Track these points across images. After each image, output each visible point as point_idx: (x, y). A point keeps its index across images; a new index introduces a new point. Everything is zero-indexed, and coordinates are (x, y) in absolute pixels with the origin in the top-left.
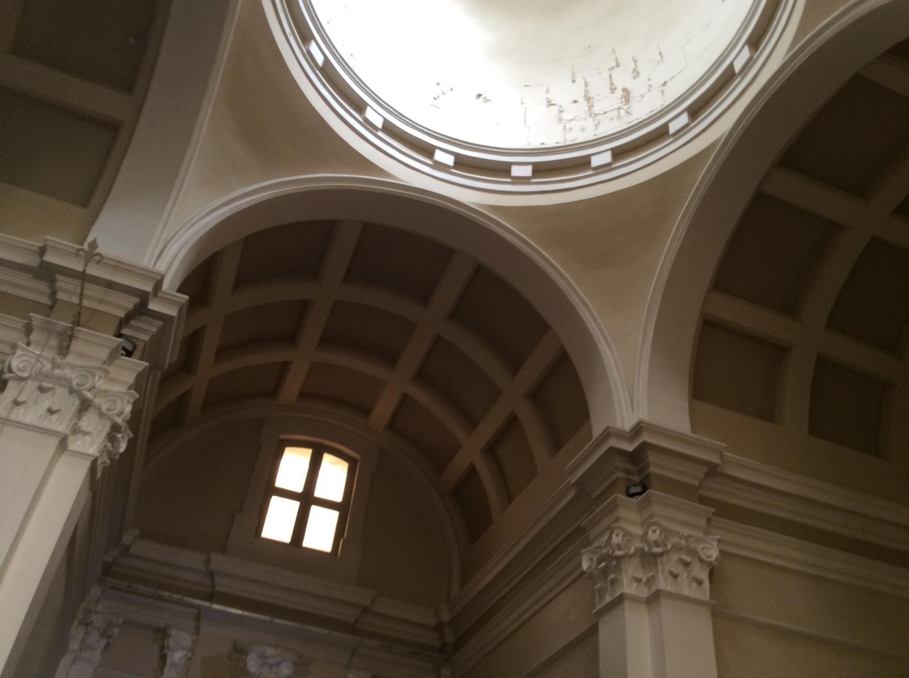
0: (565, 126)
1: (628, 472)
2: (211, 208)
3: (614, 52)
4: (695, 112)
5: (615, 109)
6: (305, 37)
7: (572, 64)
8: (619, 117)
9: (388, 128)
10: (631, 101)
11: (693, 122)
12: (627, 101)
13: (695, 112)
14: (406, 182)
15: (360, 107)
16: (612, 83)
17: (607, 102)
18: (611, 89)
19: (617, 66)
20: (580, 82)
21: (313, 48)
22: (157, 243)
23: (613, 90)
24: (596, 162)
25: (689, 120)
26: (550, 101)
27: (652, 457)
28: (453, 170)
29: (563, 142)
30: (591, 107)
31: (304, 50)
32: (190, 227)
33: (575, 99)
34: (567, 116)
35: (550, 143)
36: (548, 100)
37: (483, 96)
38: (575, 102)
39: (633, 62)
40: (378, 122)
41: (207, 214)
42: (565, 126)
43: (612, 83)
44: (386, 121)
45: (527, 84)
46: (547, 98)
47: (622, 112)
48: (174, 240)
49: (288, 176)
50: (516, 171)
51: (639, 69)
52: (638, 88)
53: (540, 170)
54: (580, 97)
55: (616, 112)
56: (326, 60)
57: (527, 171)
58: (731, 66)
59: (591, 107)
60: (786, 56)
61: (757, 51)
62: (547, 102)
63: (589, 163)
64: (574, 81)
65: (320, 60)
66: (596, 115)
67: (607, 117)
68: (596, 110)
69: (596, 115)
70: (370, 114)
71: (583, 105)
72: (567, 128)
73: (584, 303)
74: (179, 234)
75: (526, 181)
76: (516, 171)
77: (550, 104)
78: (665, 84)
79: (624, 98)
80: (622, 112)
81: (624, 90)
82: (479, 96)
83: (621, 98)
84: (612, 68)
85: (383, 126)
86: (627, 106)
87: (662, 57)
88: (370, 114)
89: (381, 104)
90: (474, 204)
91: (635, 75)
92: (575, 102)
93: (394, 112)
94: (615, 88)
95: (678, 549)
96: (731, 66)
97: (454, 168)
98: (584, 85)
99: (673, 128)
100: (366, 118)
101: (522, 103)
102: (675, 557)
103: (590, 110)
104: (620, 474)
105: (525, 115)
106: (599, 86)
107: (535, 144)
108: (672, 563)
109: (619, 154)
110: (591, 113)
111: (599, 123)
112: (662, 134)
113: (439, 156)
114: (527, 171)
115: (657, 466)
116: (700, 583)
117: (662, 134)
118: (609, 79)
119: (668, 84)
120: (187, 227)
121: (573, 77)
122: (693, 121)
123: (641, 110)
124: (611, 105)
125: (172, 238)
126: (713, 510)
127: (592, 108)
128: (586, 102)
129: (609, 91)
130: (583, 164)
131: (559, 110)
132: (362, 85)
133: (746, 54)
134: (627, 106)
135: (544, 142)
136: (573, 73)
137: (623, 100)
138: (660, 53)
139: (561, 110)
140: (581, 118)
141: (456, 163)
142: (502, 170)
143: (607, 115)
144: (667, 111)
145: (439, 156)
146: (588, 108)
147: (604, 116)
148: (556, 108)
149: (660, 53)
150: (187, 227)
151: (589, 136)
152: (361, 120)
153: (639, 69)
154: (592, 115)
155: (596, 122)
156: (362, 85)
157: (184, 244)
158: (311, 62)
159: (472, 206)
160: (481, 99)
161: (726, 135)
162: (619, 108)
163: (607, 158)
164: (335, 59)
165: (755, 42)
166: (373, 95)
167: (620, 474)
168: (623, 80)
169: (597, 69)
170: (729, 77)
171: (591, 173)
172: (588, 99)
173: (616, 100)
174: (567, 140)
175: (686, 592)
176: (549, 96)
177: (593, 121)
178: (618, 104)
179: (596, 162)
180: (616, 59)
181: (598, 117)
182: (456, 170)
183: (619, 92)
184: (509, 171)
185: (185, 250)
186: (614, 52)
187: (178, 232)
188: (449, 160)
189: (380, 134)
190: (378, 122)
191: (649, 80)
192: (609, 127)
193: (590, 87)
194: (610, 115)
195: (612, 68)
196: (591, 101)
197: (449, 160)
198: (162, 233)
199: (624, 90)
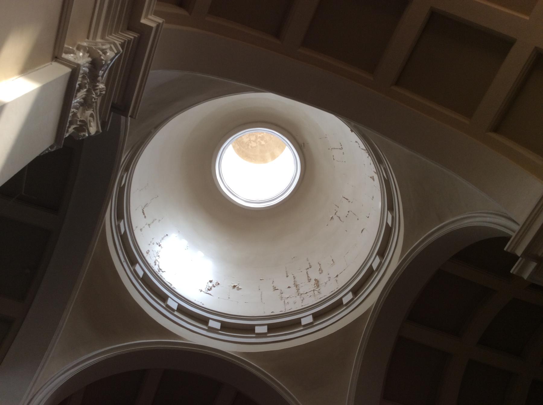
0: (284, 301)
2: (66, 369)
3: (308, 260)
4: (356, 291)
5: (312, 291)
6: (133, 262)
7: (286, 267)
8: (315, 295)
9: (180, 309)
10: (320, 286)
11: (356, 297)
12: (318, 286)
13: (356, 291)
14: (191, 341)
15: (164, 298)
16: (308, 277)
17: (307, 287)
18: (308, 280)
19: (310, 267)
20: (291, 276)
21: (137, 268)
22: (29, 394)
23: (309, 280)
24: (304, 322)
25: (353, 296)
26: (275, 288)
28: (220, 332)
29: (284, 311)
30: (298, 290)
31: (132, 270)
32: (51, 383)
33: (289, 286)
34: (285, 295)
35: (277, 312)
36: (274, 287)
37: (237, 287)
38: (289, 287)
39: (319, 265)
40: (175, 306)
41: (63, 374)
42: (284, 301)
43: (308, 277)
44: (179, 305)
45: (262, 279)
46: (273, 286)
47: (316, 292)
48: (38, 394)
49: (117, 344)
50: (258, 330)
51: (322, 269)
52: (323, 279)
53: (272, 328)
54: (292, 285)
55: (312, 292)
56: (145, 273)
57: (264, 329)
58: (371, 266)
59: (298, 290)
60: (399, 261)
61: (383, 259)
62: (274, 288)
63: (300, 323)
64: (287, 276)
65: (141, 274)
66: (301, 294)
67: (308, 295)
68: (301, 291)
69: (301, 294)
70: (170, 302)
71: (294, 289)
72: (286, 302)
74: (42, 390)
75: (265, 335)
76: (258, 330)
77: (275, 289)
78: (337, 276)
79: (316, 284)
80: (316, 292)
81: (315, 280)
82: (234, 286)
83: (315, 285)
84: (308, 269)
85: (178, 308)
86: (318, 289)
87: (334, 262)
88: (170, 302)
89: (135, 344)
90: (232, 352)
91: (321, 272)
92: (289, 287)
93: (184, 299)
94: (310, 279)
96: (371, 266)
97: (220, 330)
98: (293, 278)
99: (345, 301)
100: (168, 304)
101: (259, 289)
103: (298, 291)
105: (261, 296)
106: (302, 279)
107: (268, 314)
109: (317, 316)
110: (298, 294)
111: (304, 299)
112: (339, 305)
113: (212, 324)
114: (264, 329)
117: (339, 305)
118: (306, 274)
119: (338, 276)
120: (49, 383)
121: (287, 274)
122: (356, 296)
123: (326, 291)
124: (309, 289)
125: (37, 392)
127: (299, 291)
128: (295, 287)
129: (307, 281)
130: (297, 323)
131: (280, 292)
132: (167, 286)
133: (378, 260)
134: (318, 289)
135: (273, 311)
136: (286, 272)
137: (316, 286)
138: (332, 260)
139: (282, 292)
140: (293, 297)
141: (221, 327)
142: (249, 330)
143: (308, 294)
144: (364, 267)
145: (212, 324)
146: (297, 291)
147: (305, 294)
148: (278, 292)
149: (332, 260)
150: (49, 383)
151: (298, 306)
152: (165, 306)
153: (323, 268)
154: (300, 294)
155: (302, 299)
156: (167, 286)
157: (47, 394)
158: (136, 276)
159: (230, 353)
160: (236, 288)
161: (375, 303)
162: (314, 290)
163: (310, 319)
164: (150, 273)
165: (382, 253)
166: (172, 291)
168: (314, 275)
169: (300, 269)
170: (370, 273)
171: (302, 328)
172: (296, 286)
173: (311, 286)
174: (286, 310)
176: (274, 284)
177: (300, 298)
178: (313, 288)
179: (304, 322)
180: (309, 264)
181: (303, 296)
182: (223, 332)
183: (313, 282)
184: (254, 330)
185: (45, 400)
186: (308, 260)
187: (41, 388)
188: (218, 326)
189: (176, 313)
190: (175, 306)
191: (328, 274)
192: (310, 301)
193: (297, 279)
194: (309, 294)
195: (308, 269)
196: (298, 287)
197: (218, 326)
198: (31, 390)
199: (315, 280)
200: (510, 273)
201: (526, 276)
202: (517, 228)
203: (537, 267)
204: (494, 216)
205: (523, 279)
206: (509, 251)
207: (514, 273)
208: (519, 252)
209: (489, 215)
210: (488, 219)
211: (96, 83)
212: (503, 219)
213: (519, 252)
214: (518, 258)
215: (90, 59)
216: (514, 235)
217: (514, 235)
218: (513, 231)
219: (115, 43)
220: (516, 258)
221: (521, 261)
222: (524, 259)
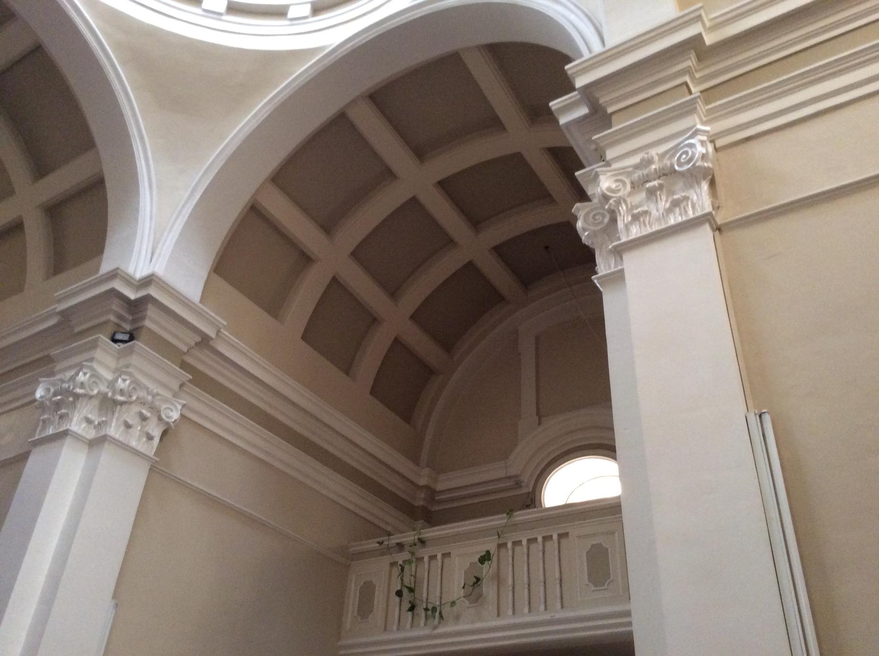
1: (120, 317)
27: (151, 311)
73: (142, 138)
95: (141, 403)
102: (135, 409)
104: (112, 318)
108: (130, 415)
115: (152, 321)
116: (150, 438)
126: (191, 377)
167: (112, 318)
175: (134, 443)
200: (549, 105)
201: (563, 120)
202: (597, 48)
203: (585, 117)
204: (582, 15)
205: (558, 122)
206: (569, 72)
207: (553, 108)
208: (580, 83)
209: (579, 13)
210: (572, 17)
211: (532, 500)
212: (592, 29)
213: (580, 83)
214: (571, 88)
215: (410, 605)
216: (586, 55)
217: (586, 55)
218: (590, 51)
219: (142, 413)
220: (571, 88)
221: (574, 96)
222: (579, 97)
